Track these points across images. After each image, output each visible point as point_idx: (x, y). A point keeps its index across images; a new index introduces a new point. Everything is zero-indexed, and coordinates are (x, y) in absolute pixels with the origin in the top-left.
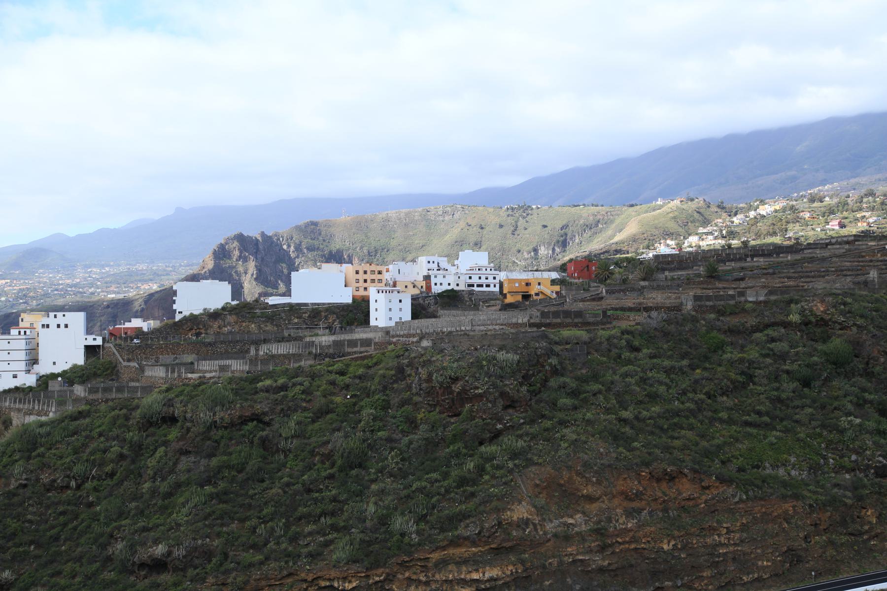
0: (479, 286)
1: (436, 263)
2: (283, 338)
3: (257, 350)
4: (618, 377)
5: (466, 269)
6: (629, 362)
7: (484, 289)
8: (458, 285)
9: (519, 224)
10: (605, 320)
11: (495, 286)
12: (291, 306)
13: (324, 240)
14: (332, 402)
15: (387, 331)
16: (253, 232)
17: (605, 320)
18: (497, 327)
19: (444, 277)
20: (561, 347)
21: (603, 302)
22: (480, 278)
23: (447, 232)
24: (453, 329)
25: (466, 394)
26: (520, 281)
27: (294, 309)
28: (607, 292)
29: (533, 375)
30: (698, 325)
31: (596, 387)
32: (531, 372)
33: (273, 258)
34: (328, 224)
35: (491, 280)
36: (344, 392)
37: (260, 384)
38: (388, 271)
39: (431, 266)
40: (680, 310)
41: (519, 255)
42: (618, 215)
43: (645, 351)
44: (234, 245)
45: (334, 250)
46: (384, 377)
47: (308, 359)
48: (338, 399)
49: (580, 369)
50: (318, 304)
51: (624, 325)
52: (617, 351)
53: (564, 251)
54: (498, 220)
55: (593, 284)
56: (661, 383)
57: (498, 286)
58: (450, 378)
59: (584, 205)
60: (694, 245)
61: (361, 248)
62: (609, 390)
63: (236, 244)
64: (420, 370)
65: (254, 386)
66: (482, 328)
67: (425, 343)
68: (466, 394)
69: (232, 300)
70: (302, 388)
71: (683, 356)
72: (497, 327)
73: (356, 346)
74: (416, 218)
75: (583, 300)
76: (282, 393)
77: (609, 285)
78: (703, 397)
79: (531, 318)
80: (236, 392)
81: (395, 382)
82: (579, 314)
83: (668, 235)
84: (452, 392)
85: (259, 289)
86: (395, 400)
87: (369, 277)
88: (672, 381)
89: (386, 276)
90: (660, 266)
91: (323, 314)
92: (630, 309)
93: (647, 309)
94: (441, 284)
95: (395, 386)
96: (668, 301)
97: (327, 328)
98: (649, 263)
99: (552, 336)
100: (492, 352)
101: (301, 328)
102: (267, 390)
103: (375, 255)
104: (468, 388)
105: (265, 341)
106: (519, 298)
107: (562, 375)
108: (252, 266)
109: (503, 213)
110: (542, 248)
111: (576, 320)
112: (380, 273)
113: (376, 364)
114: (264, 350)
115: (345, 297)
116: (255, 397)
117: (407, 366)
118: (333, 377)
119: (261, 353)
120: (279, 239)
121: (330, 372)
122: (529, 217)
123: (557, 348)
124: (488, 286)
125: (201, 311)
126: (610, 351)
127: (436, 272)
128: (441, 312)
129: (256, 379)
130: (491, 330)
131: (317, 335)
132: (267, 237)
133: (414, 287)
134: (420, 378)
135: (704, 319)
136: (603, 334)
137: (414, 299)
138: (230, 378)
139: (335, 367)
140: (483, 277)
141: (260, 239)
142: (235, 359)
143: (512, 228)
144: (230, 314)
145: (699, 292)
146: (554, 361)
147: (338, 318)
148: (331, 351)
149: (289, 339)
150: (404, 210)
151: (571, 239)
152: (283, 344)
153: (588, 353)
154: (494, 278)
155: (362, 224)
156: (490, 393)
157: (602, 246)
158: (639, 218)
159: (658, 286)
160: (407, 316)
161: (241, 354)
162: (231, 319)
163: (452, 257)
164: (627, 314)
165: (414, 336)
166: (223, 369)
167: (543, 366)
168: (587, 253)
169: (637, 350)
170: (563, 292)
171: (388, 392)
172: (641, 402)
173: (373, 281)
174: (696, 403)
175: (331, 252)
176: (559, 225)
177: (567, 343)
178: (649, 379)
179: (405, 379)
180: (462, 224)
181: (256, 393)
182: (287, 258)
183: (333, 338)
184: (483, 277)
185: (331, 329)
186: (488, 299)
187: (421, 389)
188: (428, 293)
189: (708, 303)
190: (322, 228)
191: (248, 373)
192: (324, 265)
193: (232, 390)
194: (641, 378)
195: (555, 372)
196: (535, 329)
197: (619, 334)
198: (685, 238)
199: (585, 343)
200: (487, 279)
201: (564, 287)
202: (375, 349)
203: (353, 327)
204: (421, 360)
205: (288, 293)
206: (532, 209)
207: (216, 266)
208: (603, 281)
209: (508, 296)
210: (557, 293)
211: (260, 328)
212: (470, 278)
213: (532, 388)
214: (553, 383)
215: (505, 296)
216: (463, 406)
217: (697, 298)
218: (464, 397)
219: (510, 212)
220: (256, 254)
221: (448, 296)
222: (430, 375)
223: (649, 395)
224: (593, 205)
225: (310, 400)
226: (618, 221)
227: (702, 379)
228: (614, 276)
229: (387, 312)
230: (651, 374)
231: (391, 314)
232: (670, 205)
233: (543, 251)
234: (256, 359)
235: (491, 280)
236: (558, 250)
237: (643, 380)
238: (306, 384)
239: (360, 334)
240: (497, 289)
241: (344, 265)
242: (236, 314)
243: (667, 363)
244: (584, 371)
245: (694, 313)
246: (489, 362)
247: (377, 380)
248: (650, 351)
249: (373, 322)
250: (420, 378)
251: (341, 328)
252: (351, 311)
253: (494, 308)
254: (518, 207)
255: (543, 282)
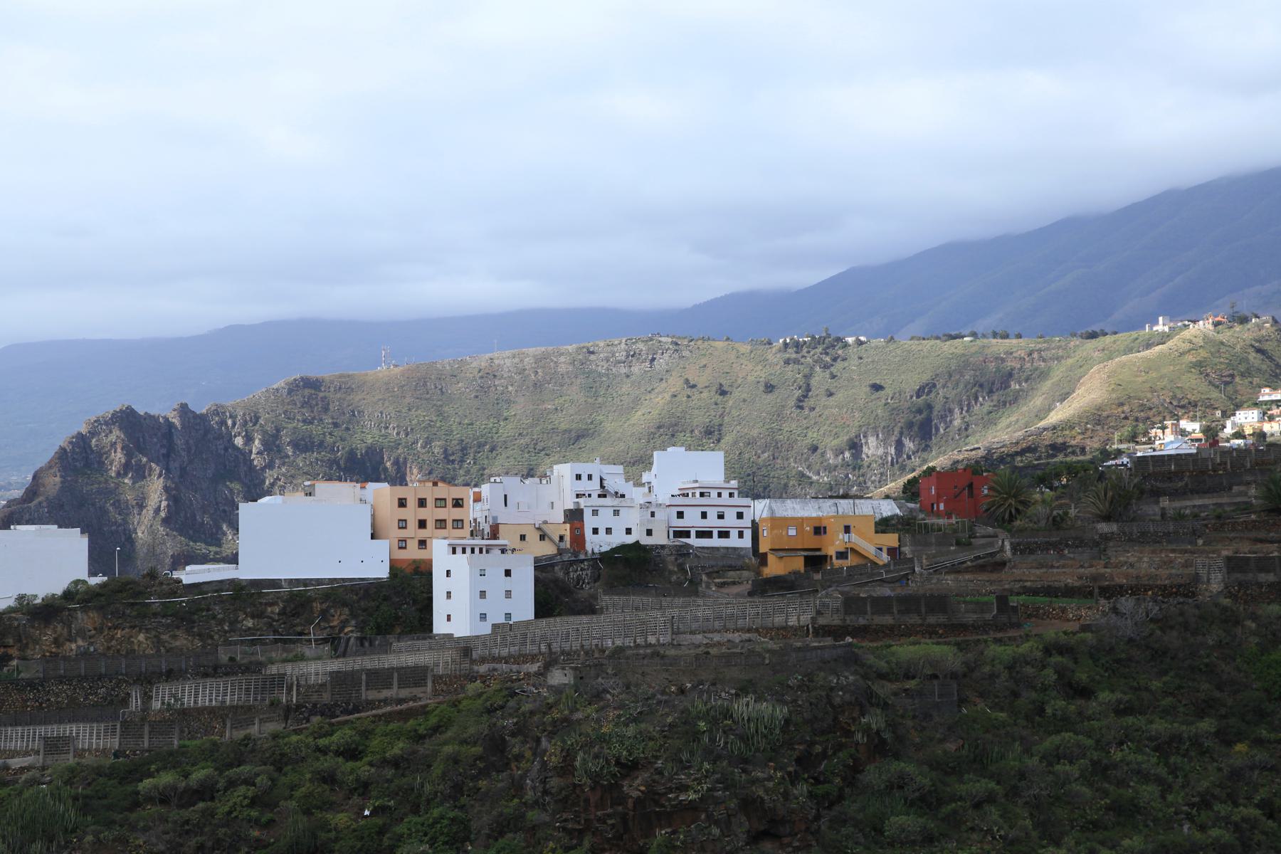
0: (703, 534)
1: (596, 480)
2: (216, 668)
3: (147, 698)
4: (1035, 761)
5: (676, 490)
6: (1064, 723)
7: (715, 542)
8: (649, 532)
9: (814, 382)
10: (1004, 618)
11: (741, 535)
12: (234, 584)
13: (336, 425)
14: (325, 826)
15: (465, 647)
16: (159, 404)
17: (1004, 618)
18: (736, 637)
19: (616, 513)
20: (894, 686)
21: (1005, 575)
22: (704, 515)
23: (637, 402)
24: (629, 642)
25: (657, 803)
26: (799, 522)
27: (247, 594)
28: (1014, 548)
29: (824, 755)
30: (1239, 630)
31: (979, 786)
32: (818, 748)
33: (206, 462)
34: (346, 386)
35: (730, 515)
36: (356, 799)
37: (147, 783)
38: (478, 499)
39: (584, 486)
40: (1194, 594)
41: (814, 458)
42: (1059, 359)
43: (1104, 696)
44: (113, 438)
45: (361, 449)
46: (456, 762)
47: (270, 720)
48: (341, 819)
49: (941, 741)
50: (305, 582)
51: (1052, 630)
52: (1034, 695)
53: (926, 448)
54: (761, 374)
55: (981, 530)
56: (1145, 777)
57: (748, 534)
58: (618, 763)
59: (974, 335)
60: (1248, 431)
61: (428, 442)
62: (1013, 793)
63: (116, 434)
64: (544, 743)
65: (129, 788)
66: (699, 638)
67: (558, 677)
68: (657, 803)
69: (92, 573)
70: (251, 791)
71: (1202, 710)
72: (736, 637)
73: (389, 686)
74: (562, 369)
75: (955, 569)
76: (201, 805)
77: (1021, 531)
78: (1254, 812)
79: (819, 613)
80: (84, 806)
81: (484, 773)
82: (939, 603)
83: (1187, 407)
84: (622, 800)
85: (172, 546)
86: (482, 819)
87: (430, 514)
88: (1173, 771)
89: (474, 512)
90: (1147, 486)
91: (317, 606)
92: (1070, 592)
93: (1111, 592)
94: (609, 531)
95: (483, 784)
96: (1164, 572)
97: (325, 641)
98: (1120, 478)
99: (871, 659)
100: (721, 699)
101: (262, 643)
102: (164, 798)
103: (460, 462)
104: (661, 789)
105: (170, 675)
106: (798, 564)
107: (897, 756)
108: (156, 489)
109: (774, 356)
110: (872, 441)
111: (932, 620)
112: (458, 503)
113: (436, 729)
114: (162, 698)
115: (373, 564)
116: (133, 816)
117: (513, 735)
118: (327, 763)
119: (156, 705)
120: (223, 423)
121: (323, 751)
122: (839, 365)
123: (884, 689)
124: (724, 534)
125: (11, 603)
126: (1016, 695)
127: (596, 501)
128: (605, 600)
129: (136, 772)
130: (719, 644)
131: (301, 658)
132: (196, 416)
133: (542, 537)
134: (544, 764)
135: (1254, 617)
136: (999, 652)
137: (542, 567)
138: (72, 770)
139: (335, 738)
140: (712, 513)
141: (176, 421)
142: (92, 720)
143: (798, 393)
144: (85, 609)
145: (1246, 549)
146: (874, 720)
147: (353, 615)
148: (326, 698)
149: (232, 669)
150: (531, 351)
151: (943, 418)
152: (209, 681)
153: (962, 701)
154: (740, 516)
155: (430, 385)
156: (717, 802)
157: (1020, 434)
158: (1111, 365)
159: (1143, 534)
160: (524, 609)
161: (108, 710)
162: (85, 620)
163: (637, 464)
164: (1061, 603)
165: (533, 658)
166: (54, 746)
167: (848, 734)
168: (981, 453)
169: (1085, 692)
170: (906, 550)
171: (464, 800)
172: (1096, 825)
173: (441, 524)
174: (1237, 828)
175: (352, 453)
176: (912, 381)
177: (908, 676)
178: (1115, 766)
179: (507, 766)
180: (675, 383)
181: (136, 805)
182: (243, 469)
183: (335, 665)
184: (712, 513)
185: (335, 643)
186: (724, 566)
187: (545, 792)
188: (575, 554)
189: (1263, 577)
190: (331, 395)
191: (116, 755)
192: (322, 487)
193: (75, 799)
194: (1094, 763)
195: (880, 748)
196: (828, 641)
197: (1039, 654)
198: (1227, 415)
199: (954, 676)
200: (721, 516)
201: (908, 538)
202: (436, 693)
203: (391, 638)
204: (548, 718)
205: (233, 559)
206: (846, 345)
207: (66, 488)
208: (1005, 521)
209: (771, 559)
210: (891, 551)
211: (158, 642)
212: (680, 515)
213: (821, 789)
214: (873, 775)
215: (763, 559)
216: (649, 834)
217: (1234, 564)
218: (652, 811)
219: (791, 354)
220: (166, 458)
221: (627, 562)
222: (569, 756)
223: (1116, 808)
224: (995, 335)
225: (271, 822)
226: (1058, 372)
227: (1252, 768)
228: (1031, 511)
229: (471, 599)
230: (1119, 756)
231: (484, 606)
232: (1186, 334)
233: (872, 448)
234: (143, 719)
235: (730, 520)
236: (909, 445)
237: (1101, 770)
238: (262, 780)
239: (404, 655)
240: (747, 542)
241: (371, 486)
242: (100, 608)
243: (1160, 726)
244: (951, 746)
245: (1227, 602)
246: (714, 722)
247: (437, 769)
248: (1118, 695)
249: (435, 631)
250: (544, 764)
251: (361, 640)
252: (386, 599)
253: (735, 590)
254: (809, 335)
255: (859, 521)
